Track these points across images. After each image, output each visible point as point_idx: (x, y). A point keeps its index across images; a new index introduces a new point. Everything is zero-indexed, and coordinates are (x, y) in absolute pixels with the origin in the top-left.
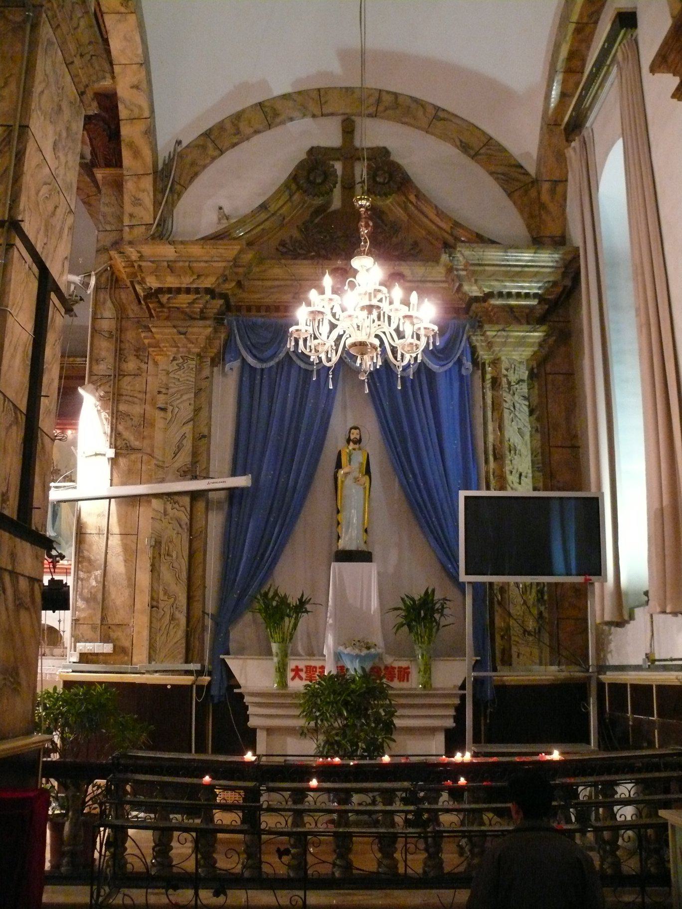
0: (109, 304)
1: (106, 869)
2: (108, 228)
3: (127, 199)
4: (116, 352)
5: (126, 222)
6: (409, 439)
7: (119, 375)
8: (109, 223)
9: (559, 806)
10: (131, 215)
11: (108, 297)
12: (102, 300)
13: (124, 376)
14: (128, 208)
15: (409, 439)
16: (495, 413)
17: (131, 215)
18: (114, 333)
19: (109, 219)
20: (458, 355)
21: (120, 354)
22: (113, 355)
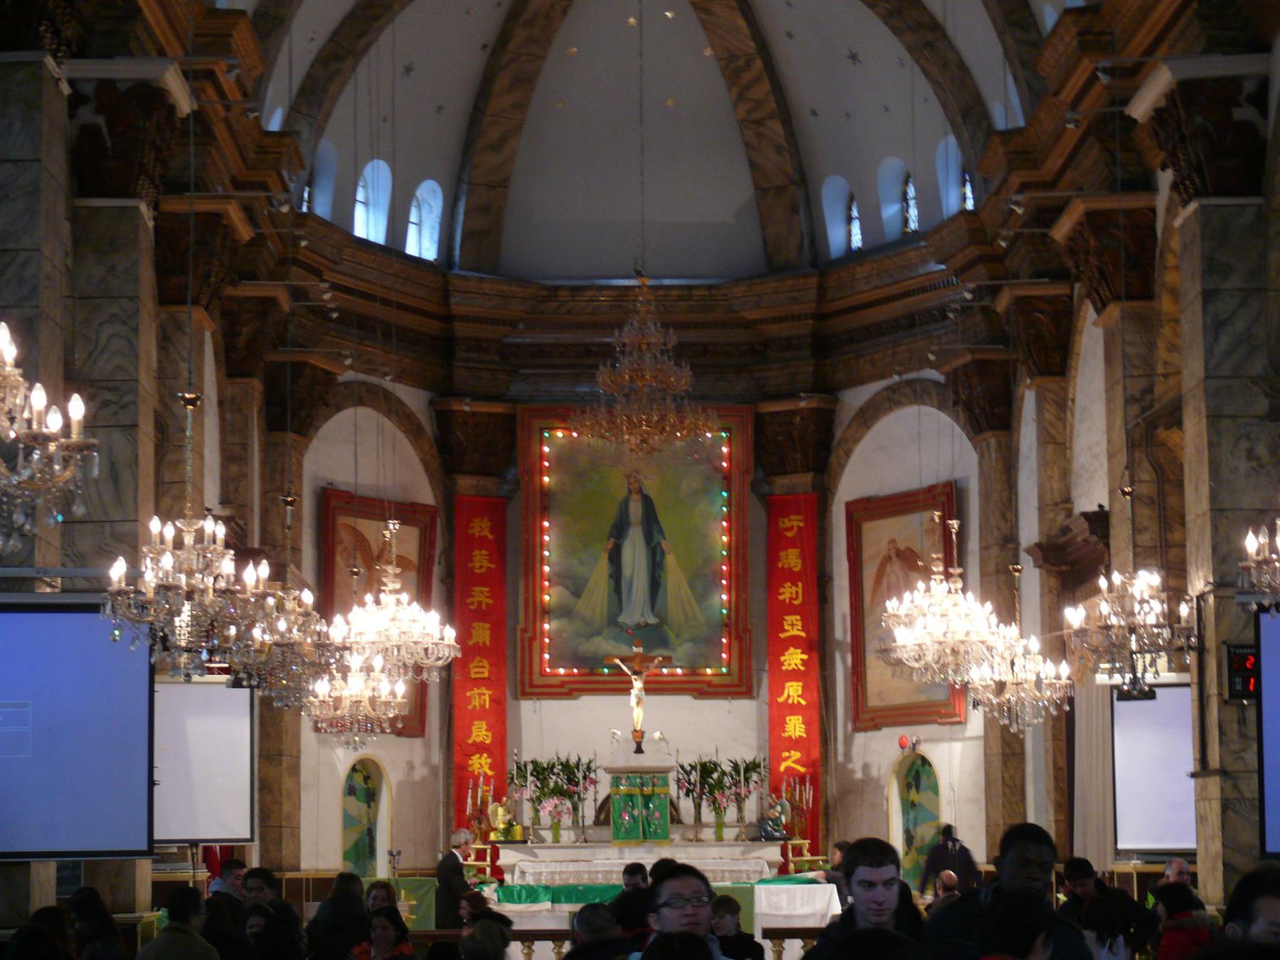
0: (1146, 465)
1: (1143, 896)
2: (1135, 373)
3: (1161, 345)
4: (1160, 520)
5: (1160, 369)
6: (470, 795)
7: (1166, 546)
8: (1136, 367)
9: (1137, 641)
10: (1166, 363)
11: (1144, 457)
12: (1137, 459)
13: (1171, 547)
14: (1162, 353)
15: (470, 795)
16: (482, 703)
17: (1166, 363)
18: (1156, 499)
19: (1136, 362)
20: (419, 878)
21: (1165, 523)
22: (1158, 522)
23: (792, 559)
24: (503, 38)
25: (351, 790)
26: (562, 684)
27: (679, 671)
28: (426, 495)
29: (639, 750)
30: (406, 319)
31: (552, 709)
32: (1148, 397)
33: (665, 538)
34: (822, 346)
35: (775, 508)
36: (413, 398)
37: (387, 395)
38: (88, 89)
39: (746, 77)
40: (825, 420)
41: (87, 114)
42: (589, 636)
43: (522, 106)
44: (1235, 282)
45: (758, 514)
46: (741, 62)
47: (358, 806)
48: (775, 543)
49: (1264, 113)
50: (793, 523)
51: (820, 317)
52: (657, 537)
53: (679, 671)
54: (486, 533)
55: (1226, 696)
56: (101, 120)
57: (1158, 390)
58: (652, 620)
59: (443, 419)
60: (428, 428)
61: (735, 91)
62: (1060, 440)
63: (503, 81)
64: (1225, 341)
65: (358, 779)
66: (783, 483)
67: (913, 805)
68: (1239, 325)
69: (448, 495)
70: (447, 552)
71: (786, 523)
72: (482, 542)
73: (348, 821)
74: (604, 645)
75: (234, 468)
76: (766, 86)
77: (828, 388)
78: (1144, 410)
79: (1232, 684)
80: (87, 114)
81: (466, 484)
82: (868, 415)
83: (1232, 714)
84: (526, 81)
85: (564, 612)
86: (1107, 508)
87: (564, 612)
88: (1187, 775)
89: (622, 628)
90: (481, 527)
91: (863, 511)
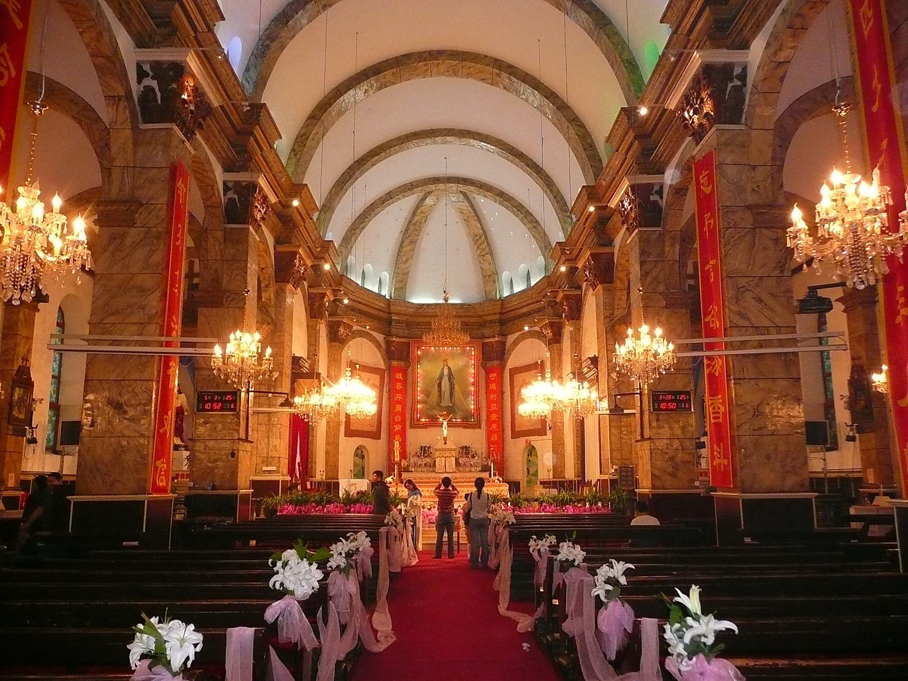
3: (617, 299)
23: (493, 386)
24: (407, 230)
25: (356, 455)
26: (423, 424)
27: (459, 420)
28: (382, 365)
29: (445, 443)
30: (376, 312)
31: (420, 431)
32: (612, 316)
33: (560, 583)
34: (502, 323)
35: (488, 372)
36: (380, 337)
37: (371, 335)
38: (230, 185)
39: (479, 242)
40: (503, 344)
41: (231, 194)
42: (431, 410)
43: (413, 250)
44: (651, 258)
45: (483, 373)
46: (478, 237)
47: (359, 461)
48: (488, 382)
49: (661, 198)
50: (493, 376)
51: (501, 313)
52: (452, 379)
53: (459, 420)
54: (401, 377)
55: (652, 410)
56: (236, 197)
57: (616, 312)
58: (451, 405)
59: (388, 343)
60: (383, 346)
61: (476, 246)
62: (578, 340)
63: (407, 242)
64: (649, 279)
65: (359, 451)
66: (489, 364)
67: (530, 461)
68: (654, 274)
69: (390, 368)
70: (389, 383)
71: (491, 376)
72: (399, 380)
73: (355, 465)
74: (436, 412)
75: (312, 348)
76: (486, 244)
77: (504, 335)
78: (611, 321)
79: (654, 406)
80: (231, 194)
81: (395, 363)
82: (516, 343)
83: (653, 417)
84: (413, 242)
85: (423, 402)
86: (597, 356)
87: (423, 402)
88: (173, 679)
89: (442, 407)
90: (399, 376)
91: (515, 371)
